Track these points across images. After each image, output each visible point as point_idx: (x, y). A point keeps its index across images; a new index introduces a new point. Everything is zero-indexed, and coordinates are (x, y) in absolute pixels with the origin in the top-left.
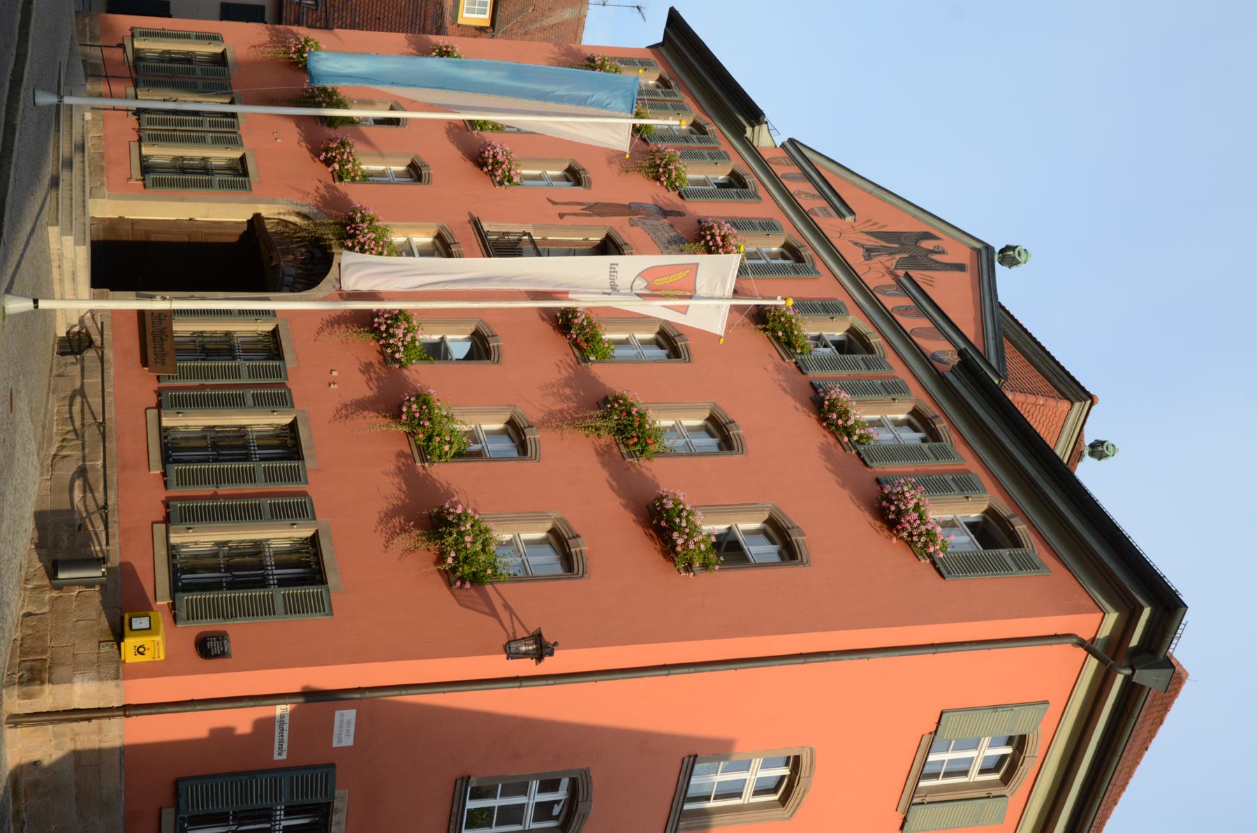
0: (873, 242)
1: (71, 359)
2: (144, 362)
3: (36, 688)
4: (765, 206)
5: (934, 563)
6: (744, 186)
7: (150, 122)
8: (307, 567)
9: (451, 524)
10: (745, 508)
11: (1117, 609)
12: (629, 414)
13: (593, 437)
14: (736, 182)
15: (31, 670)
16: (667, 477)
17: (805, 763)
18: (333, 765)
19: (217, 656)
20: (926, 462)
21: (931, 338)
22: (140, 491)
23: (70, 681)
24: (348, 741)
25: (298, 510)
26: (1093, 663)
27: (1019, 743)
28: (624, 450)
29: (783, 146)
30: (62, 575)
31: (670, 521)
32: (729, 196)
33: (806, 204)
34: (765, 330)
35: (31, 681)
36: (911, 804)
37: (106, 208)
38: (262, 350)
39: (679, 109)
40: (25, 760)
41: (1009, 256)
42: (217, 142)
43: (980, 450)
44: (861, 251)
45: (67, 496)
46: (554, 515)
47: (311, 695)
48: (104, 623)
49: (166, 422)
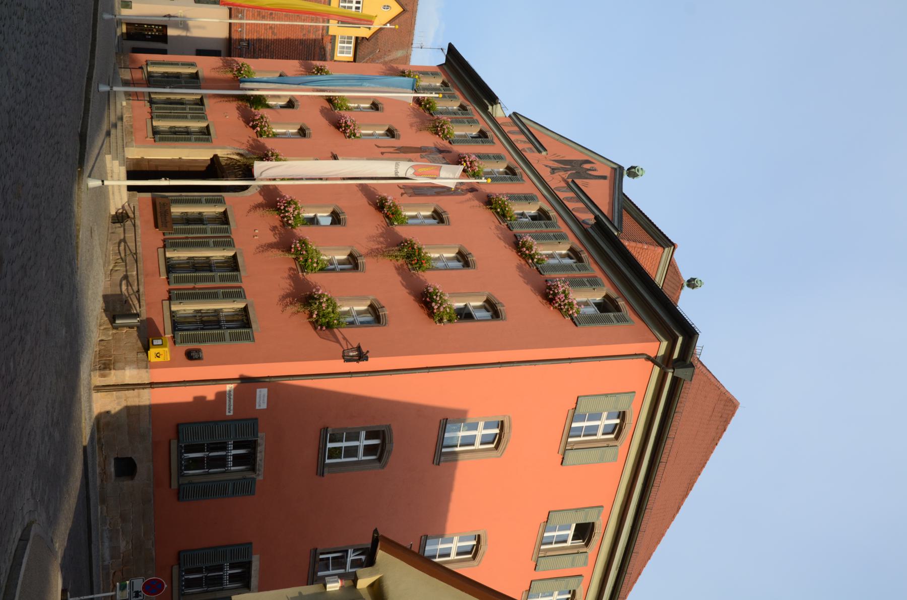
0: (556, 165)
1: (118, 225)
2: (156, 226)
3: (107, 372)
4: (497, 147)
5: (572, 319)
6: (486, 137)
7: (157, 108)
8: (243, 320)
9: (316, 299)
11: (667, 339)
12: (413, 248)
13: (394, 261)
14: (482, 135)
15: (104, 364)
17: (506, 425)
19: (196, 359)
20: (574, 272)
21: (585, 212)
23: (124, 369)
24: (264, 406)
25: (238, 294)
26: (657, 369)
27: (622, 416)
28: (410, 267)
29: (510, 116)
30: (118, 322)
31: (431, 298)
32: (477, 142)
33: (520, 146)
34: (491, 208)
35: (105, 368)
36: (565, 450)
37: (135, 153)
38: (227, 267)
39: (452, 97)
40: (103, 410)
41: (633, 172)
42: (194, 118)
43: (604, 266)
46: (371, 297)
48: (140, 344)
49: (168, 255)
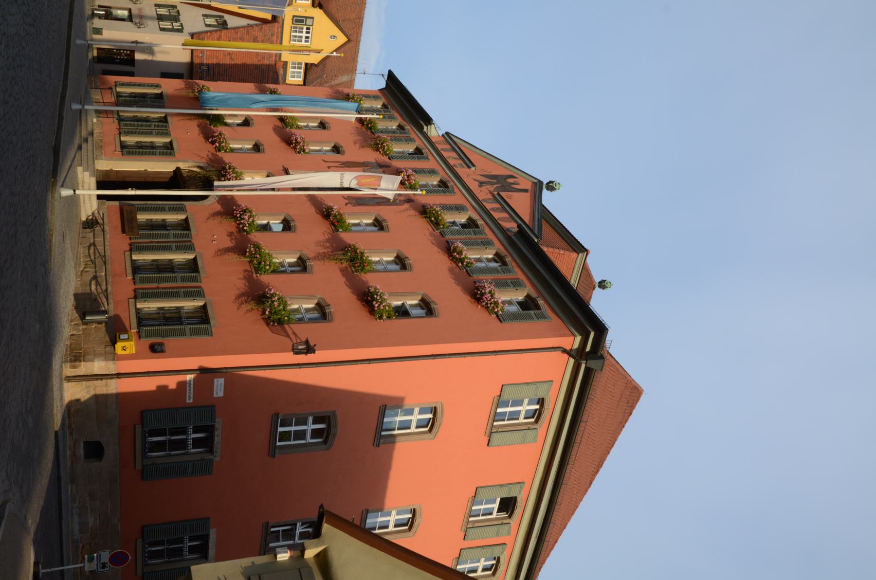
0: (484, 179)
1: (88, 230)
2: (123, 231)
3: (77, 363)
5: (497, 316)
6: (422, 154)
7: (125, 125)
8: (202, 316)
9: (269, 298)
10: (411, 294)
11: (580, 334)
12: (356, 253)
13: (339, 264)
14: (418, 152)
15: (75, 356)
16: (372, 280)
17: (439, 410)
18: (214, 406)
19: (159, 352)
21: (508, 221)
22: (124, 286)
23: (93, 361)
24: (221, 394)
25: (197, 293)
27: (541, 402)
31: (372, 297)
32: (413, 158)
33: (452, 162)
35: (75, 361)
36: (491, 432)
37: (104, 165)
39: (391, 118)
40: (73, 398)
43: (525, 269)
44: (477, 183)
45: (88, 288)
46: (319, 296)
47: (203, 370)
48: (107, 338)
